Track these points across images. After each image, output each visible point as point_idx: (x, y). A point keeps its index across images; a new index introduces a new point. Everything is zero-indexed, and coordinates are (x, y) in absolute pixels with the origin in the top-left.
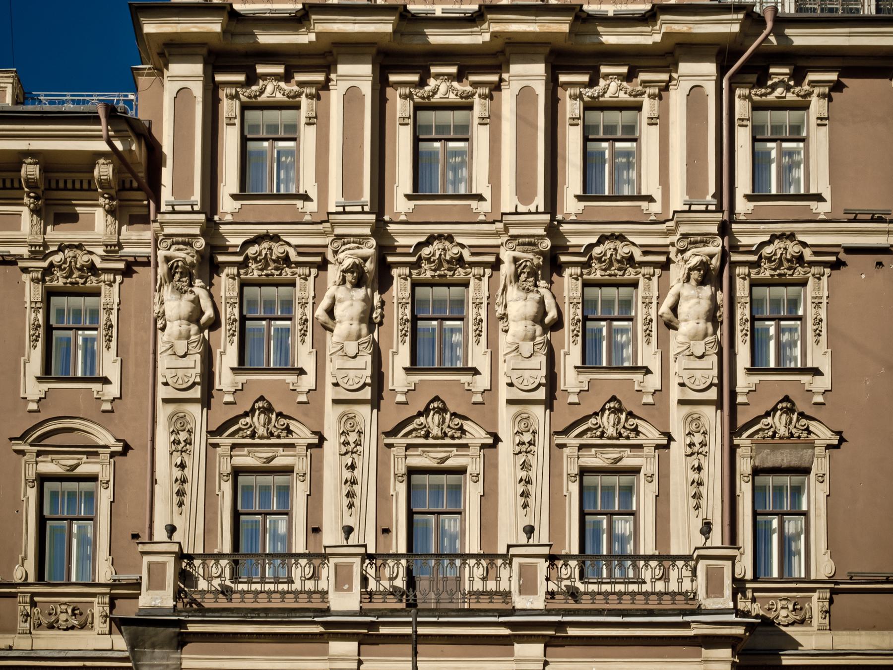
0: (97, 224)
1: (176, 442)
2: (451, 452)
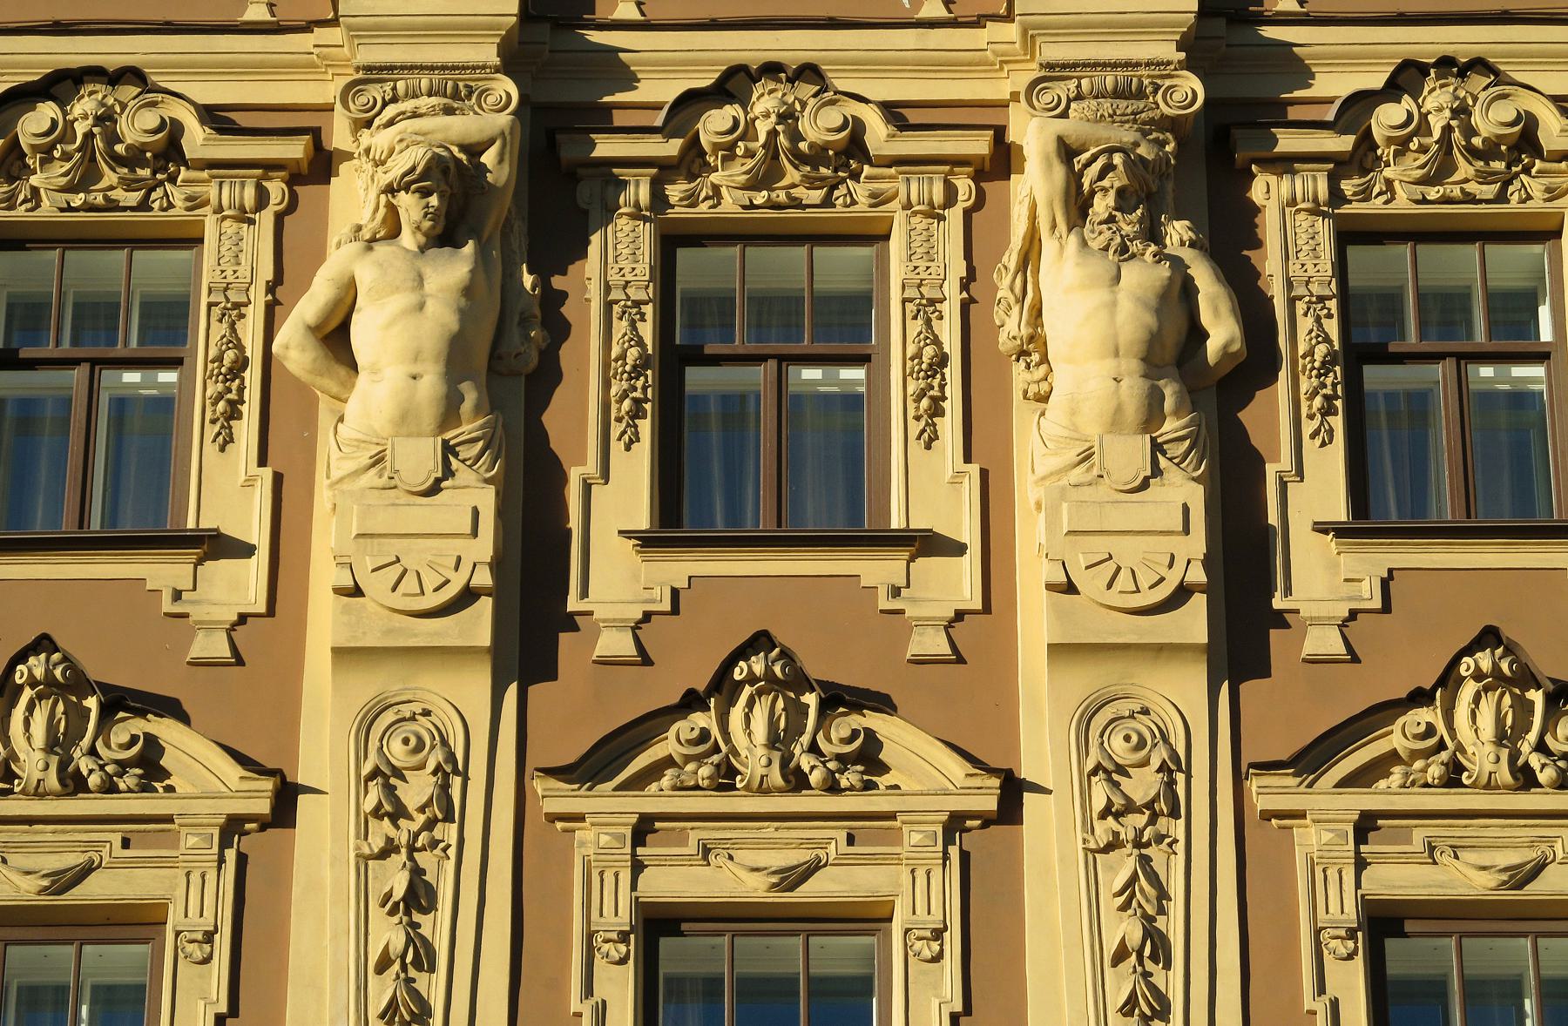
2: (823, 844)
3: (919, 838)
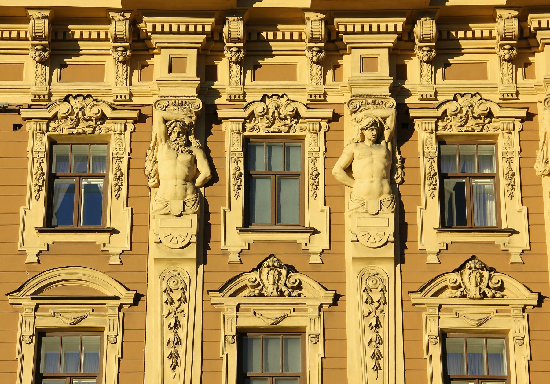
3: (314, 311)
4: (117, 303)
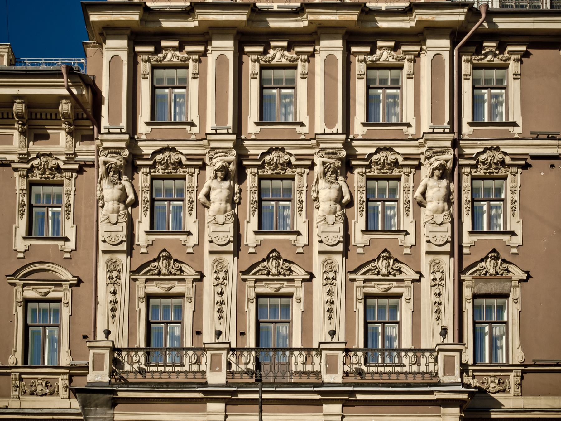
0: (61, 141)
1: (111, 278)
2: (283, 284)
4: (68, 283)
